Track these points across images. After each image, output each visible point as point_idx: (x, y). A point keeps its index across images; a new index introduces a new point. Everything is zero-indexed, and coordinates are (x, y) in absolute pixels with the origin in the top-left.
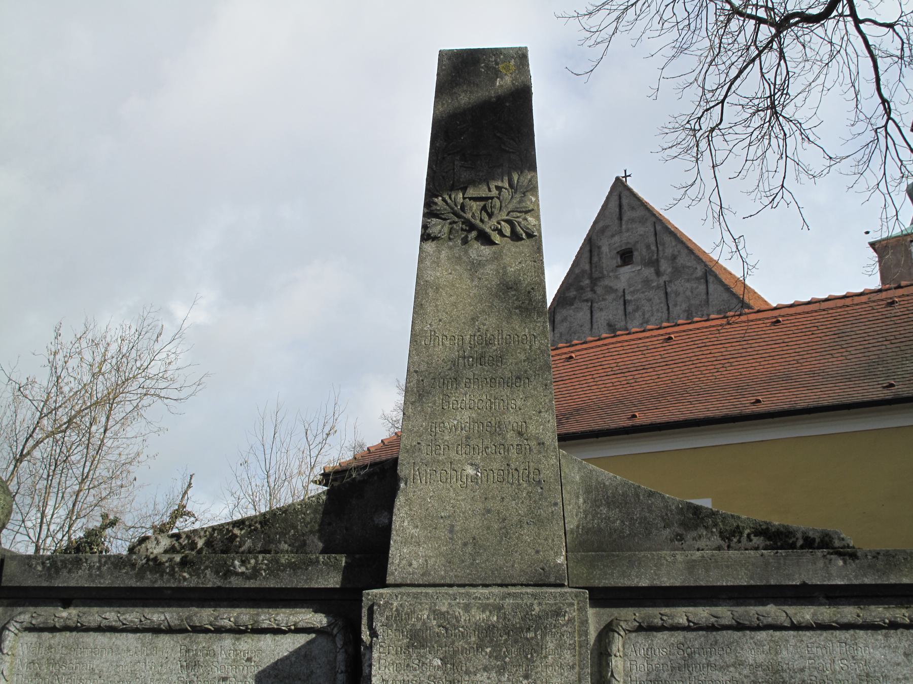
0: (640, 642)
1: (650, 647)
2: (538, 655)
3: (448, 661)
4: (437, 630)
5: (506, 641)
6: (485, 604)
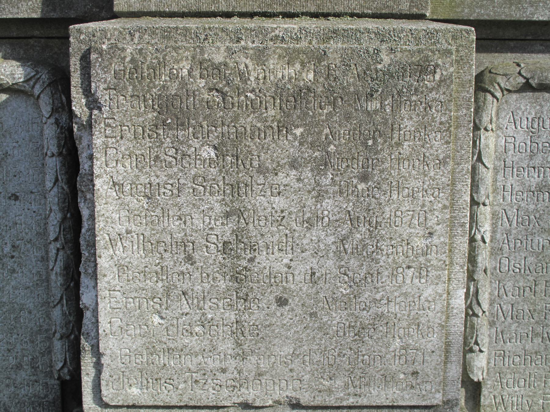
0: (523, 108)
1: (538, 115)
2: (385, 141)
3: (227, 151)
4: (206, 96)
5: (330, 114)
6: (294, 50)
